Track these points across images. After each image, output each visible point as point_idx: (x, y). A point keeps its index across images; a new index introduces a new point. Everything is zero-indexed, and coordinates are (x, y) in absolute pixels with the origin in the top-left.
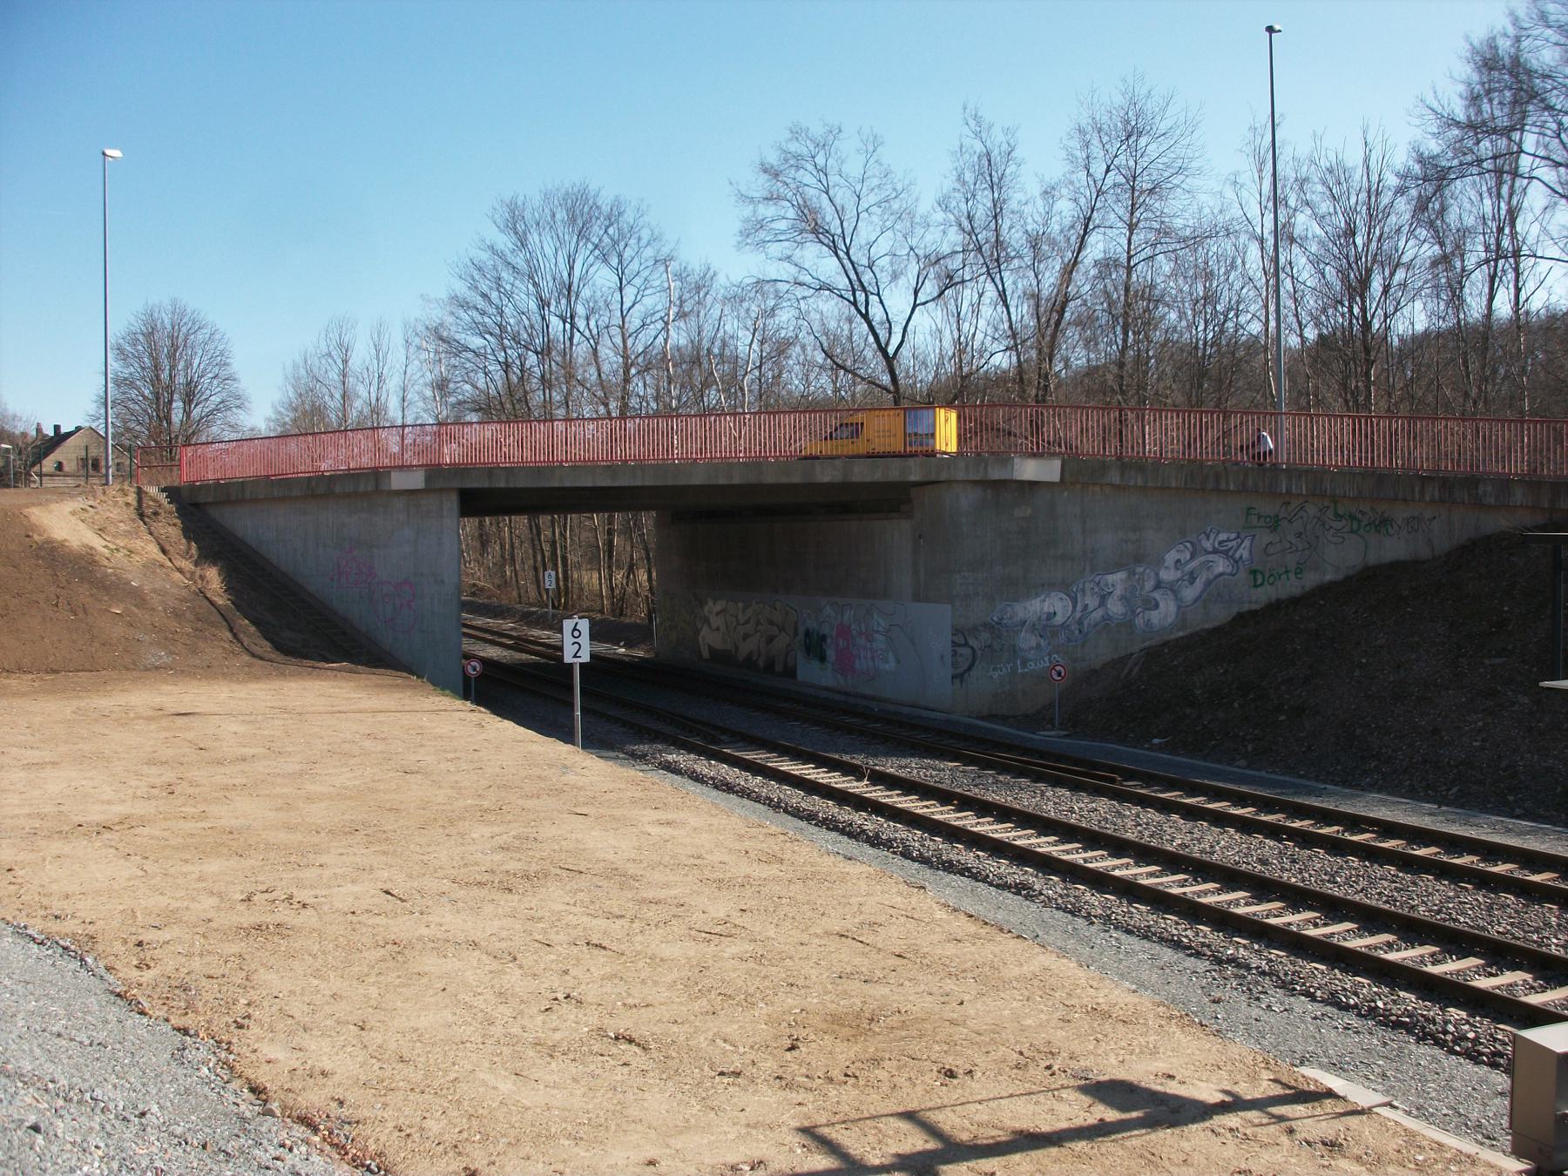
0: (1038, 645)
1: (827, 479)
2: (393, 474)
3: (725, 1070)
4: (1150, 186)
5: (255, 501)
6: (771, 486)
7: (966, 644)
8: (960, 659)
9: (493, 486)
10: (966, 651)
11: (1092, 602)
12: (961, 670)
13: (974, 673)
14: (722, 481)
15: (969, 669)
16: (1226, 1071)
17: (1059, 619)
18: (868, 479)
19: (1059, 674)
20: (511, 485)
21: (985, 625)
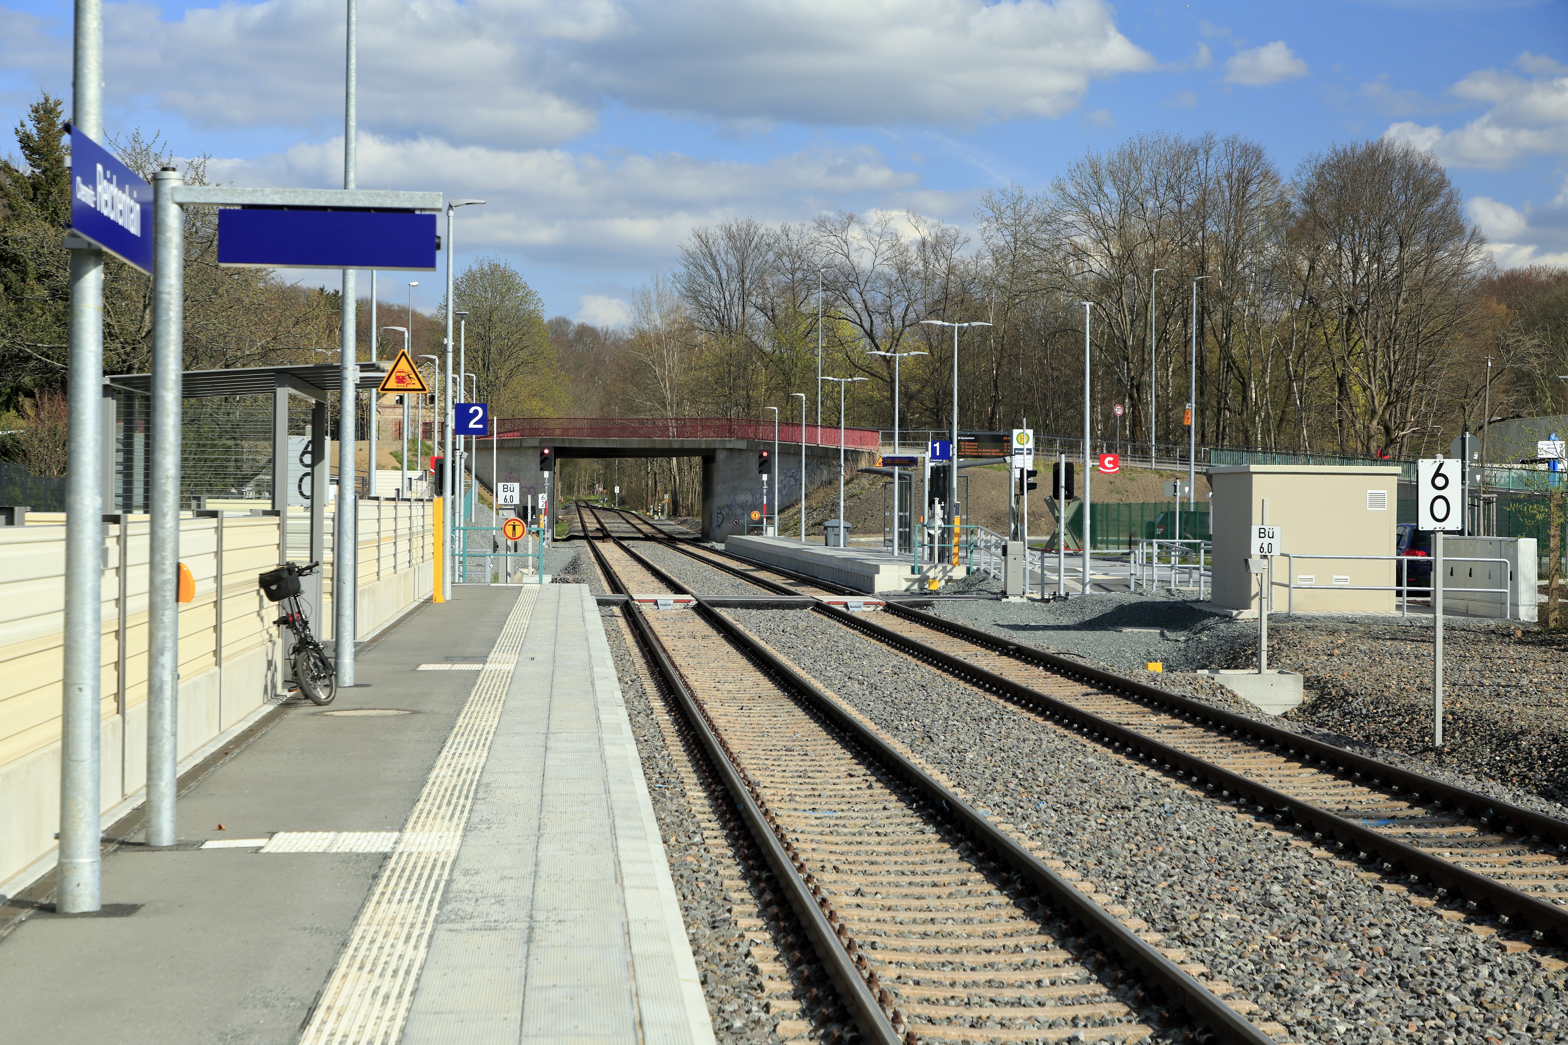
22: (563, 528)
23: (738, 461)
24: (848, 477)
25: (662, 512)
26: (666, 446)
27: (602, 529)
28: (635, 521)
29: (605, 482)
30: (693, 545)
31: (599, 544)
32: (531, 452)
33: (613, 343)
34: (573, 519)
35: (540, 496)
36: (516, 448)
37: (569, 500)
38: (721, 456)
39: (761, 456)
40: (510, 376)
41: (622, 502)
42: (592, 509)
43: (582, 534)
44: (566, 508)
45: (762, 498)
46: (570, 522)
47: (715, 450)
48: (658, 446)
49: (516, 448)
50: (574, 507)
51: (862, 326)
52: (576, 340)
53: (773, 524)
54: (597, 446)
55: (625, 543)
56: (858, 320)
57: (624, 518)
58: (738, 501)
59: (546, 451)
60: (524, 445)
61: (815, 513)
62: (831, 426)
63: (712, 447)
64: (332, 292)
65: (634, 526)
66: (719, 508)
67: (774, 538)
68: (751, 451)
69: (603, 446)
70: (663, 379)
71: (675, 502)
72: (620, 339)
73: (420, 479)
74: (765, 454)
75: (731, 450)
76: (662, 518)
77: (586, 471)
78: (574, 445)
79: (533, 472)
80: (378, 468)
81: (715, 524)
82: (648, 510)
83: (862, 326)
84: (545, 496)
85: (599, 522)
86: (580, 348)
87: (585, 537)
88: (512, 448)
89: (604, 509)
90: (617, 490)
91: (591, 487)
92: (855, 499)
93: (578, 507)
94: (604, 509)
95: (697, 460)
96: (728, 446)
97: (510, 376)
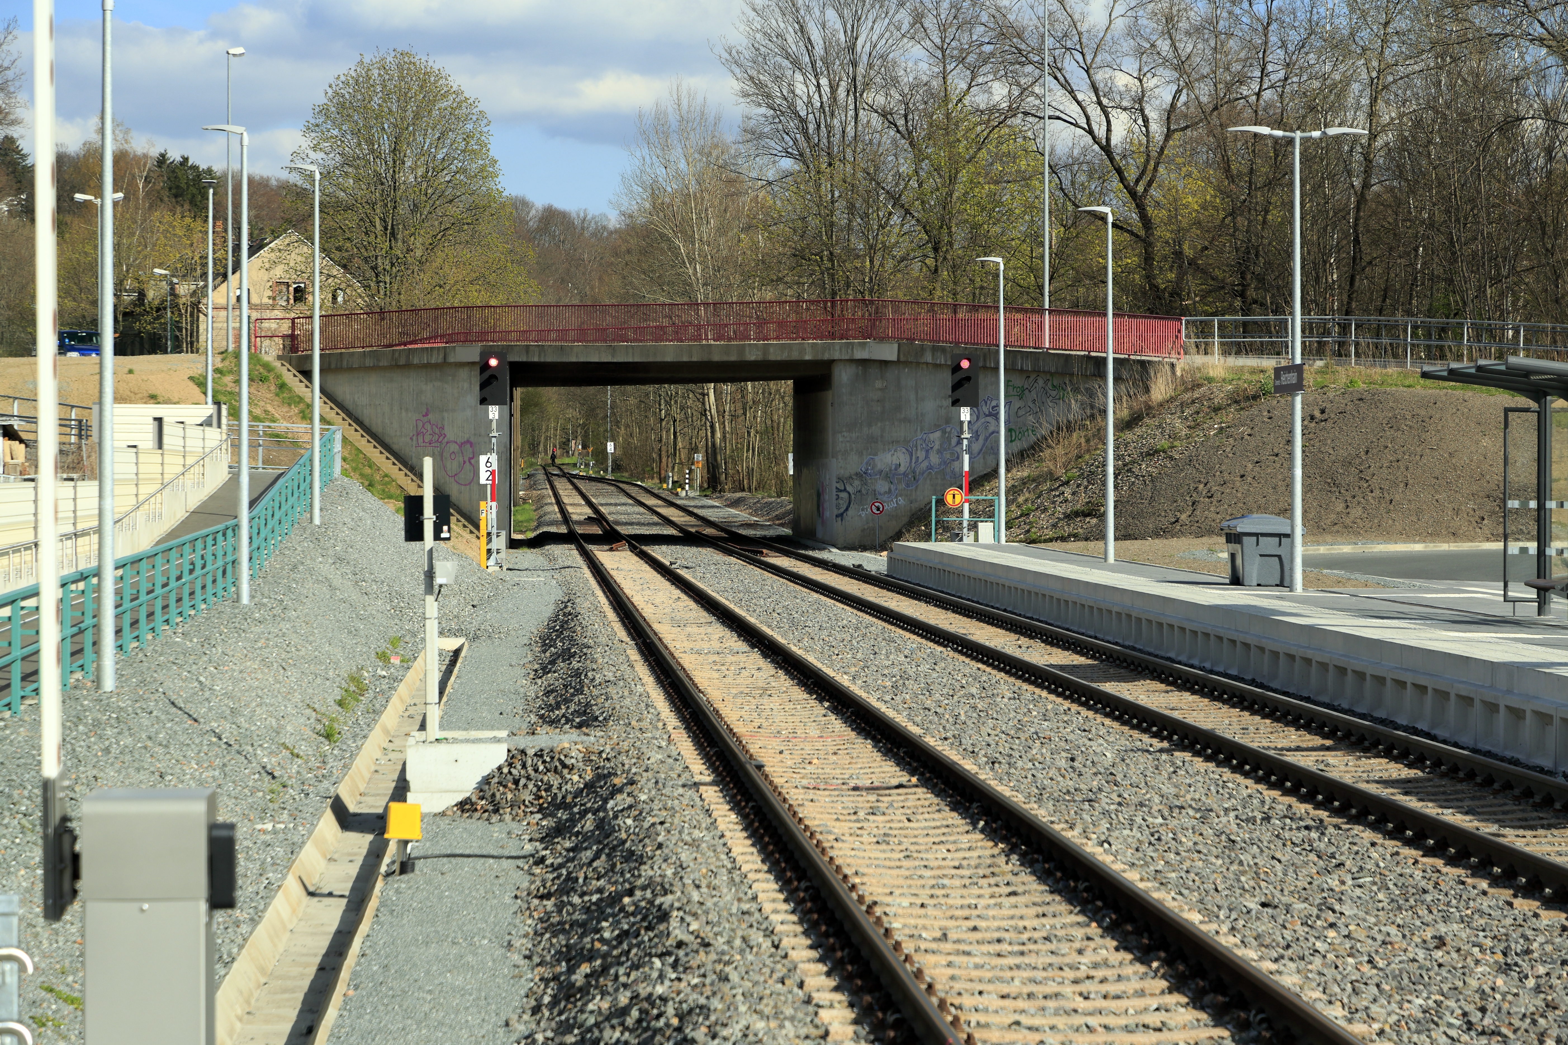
0: (890, 490)
1: (753, 358)
2: (980, 524)
3: (860, 783)
4: (1401, 923)
5: (350, 369)
6: (717, 362)
7: (845, 490)
8: (841, 502)
9: (530, 360)
10: (844, 495)
11: (921, 454)
12: (842, 510)
13: (850, 512)
14: (685, 359)
15: (847, 509)
16: (1003, 873)
17: (902, 469)
18: (779, 358)
19: (878, 509)
20: (542, 360)
21: (857, 474)
22: (525, 514)
23: (879, 384)
24: (1125, 413)
25: (691, 487)
26: (733, 358)
27: (599, 518)
28: (651, 501)
29: (585, 436)
30: (787, 554)
31: (605, 557)
32: (464, 373)
33: (594, 235)
34: (541, 498)
35: (483, 459)
36: (436, 366)
37: (532, 465)
38: (843, 376)
39: (957, 368)
40: (431, 247)
41: (617, 467)
42: (570, 478)
43: (563, 530)
44: (529, 476)
45: (959, 458)
46: (540, 503)
47: (830, 363)
48: (716, 358)
49: (436, 366)
50: (541, 476)
51: (1090, 132)
52: (538, 230)
53: (990, 515)
54: (595, 359)
55: (650, 550)
56: (1082, 122)
57: (631, 497)
58: (880, 466)
59: (493, 362)
60: (451, 359)
61: (1068, 492)
62: (1076, 309)
63: (826, 357)
64: (179, 159)
65: (650, 509)
66: (840, 479)
67: (996, 547)
68: (906, 363)
69: (606, 358)
70: (692, 261)
71: (712, 468)
72: (604, 228)
73: (208, 423)
74: (965, 364)
75: (864, 363)
76: (691, 494)
77: (557, 419)
78: (550, 358)
79: (469, 413)
80: (119, 399)
81: (830, 511)
82: (664, 480)
83: (1090, 132)
84: (494, 458)
85: (590, 504)
86: (546, 241)
87: (570, 538)
88: (428, 366)
89: (590, 479)
90: (610, 447)
91: (565, 445)
92: (1160, 460)
93: (549, 476)
94: (590, 479)
95: (787, 386)
96: (859, 355)
97: (431, 247)
